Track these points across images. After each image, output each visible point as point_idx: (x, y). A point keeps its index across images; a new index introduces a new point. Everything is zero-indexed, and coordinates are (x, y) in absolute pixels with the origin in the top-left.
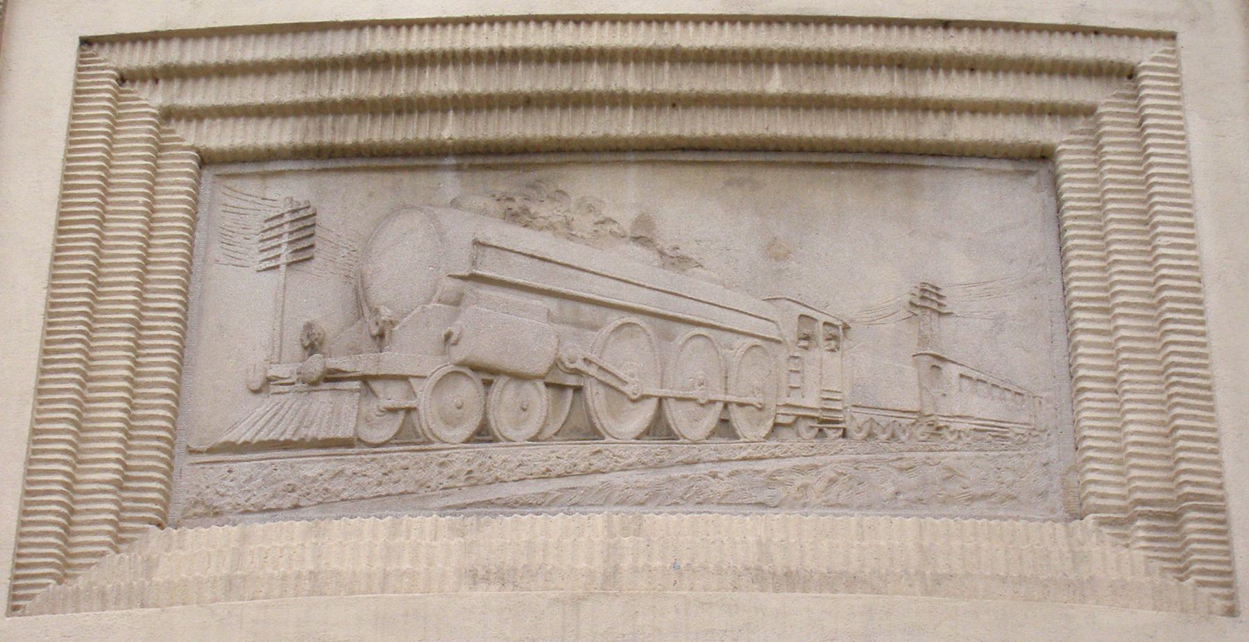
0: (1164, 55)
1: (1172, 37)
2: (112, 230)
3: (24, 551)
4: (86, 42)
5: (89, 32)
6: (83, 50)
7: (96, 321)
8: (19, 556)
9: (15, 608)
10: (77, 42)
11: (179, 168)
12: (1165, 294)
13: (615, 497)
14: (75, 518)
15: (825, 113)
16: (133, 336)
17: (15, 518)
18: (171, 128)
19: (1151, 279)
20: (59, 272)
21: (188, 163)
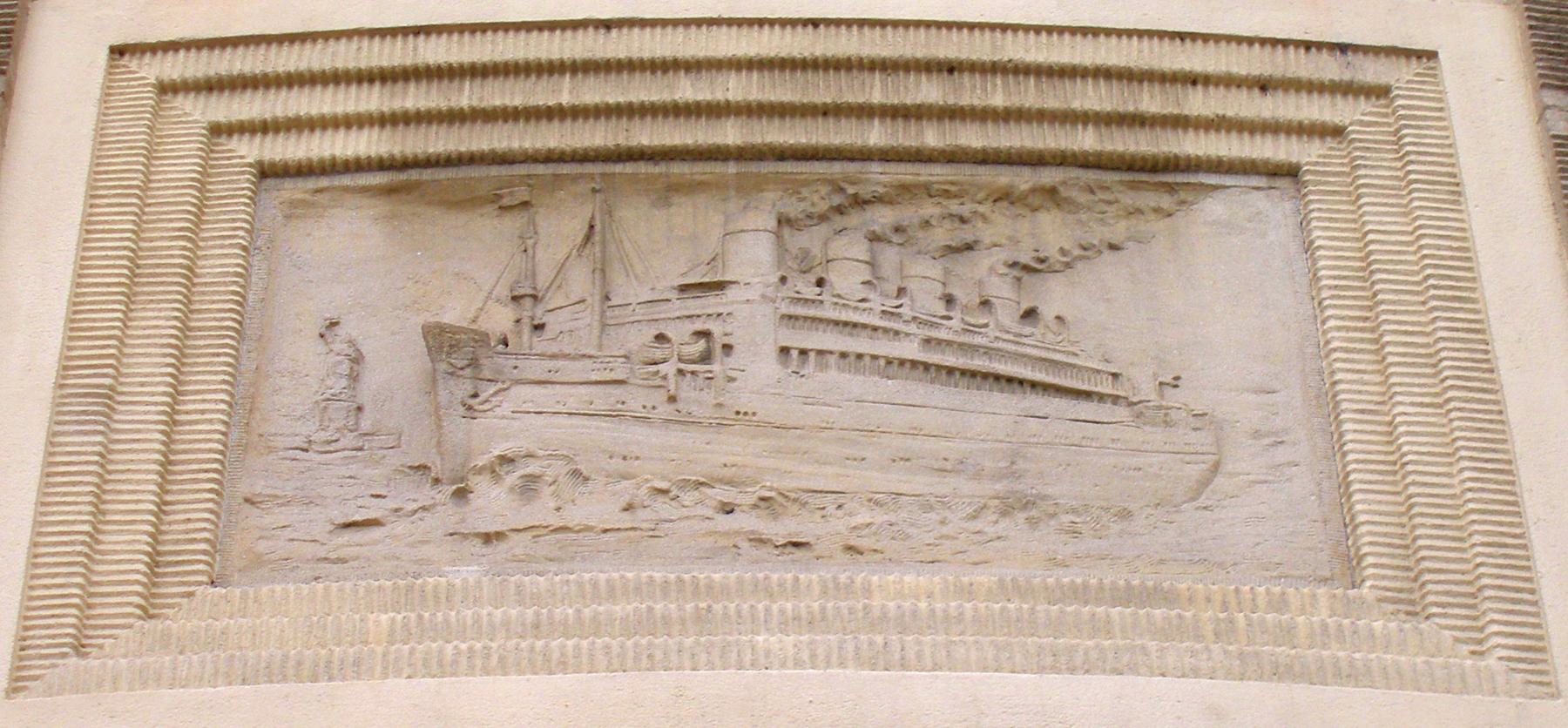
0: (1426, 72)
1: (1432, 55)
2: (117, 463)
3: (58, 439)
4: (118, 51)
5: (119, 40)
6: (113, 60)
7: (105, 492)
8: (79, 285)
9: (16, 690)
10: (107, 51)
11: (235, 185)
12: (1372, 247)
13: (646, 157)
14: (131, 315)
15: (1023, 126)
16: (157, 500)
17: (42, 447)
18: (220, 141)
19: (1358, 235)
20: (84, 280)
21: (245, 181)
